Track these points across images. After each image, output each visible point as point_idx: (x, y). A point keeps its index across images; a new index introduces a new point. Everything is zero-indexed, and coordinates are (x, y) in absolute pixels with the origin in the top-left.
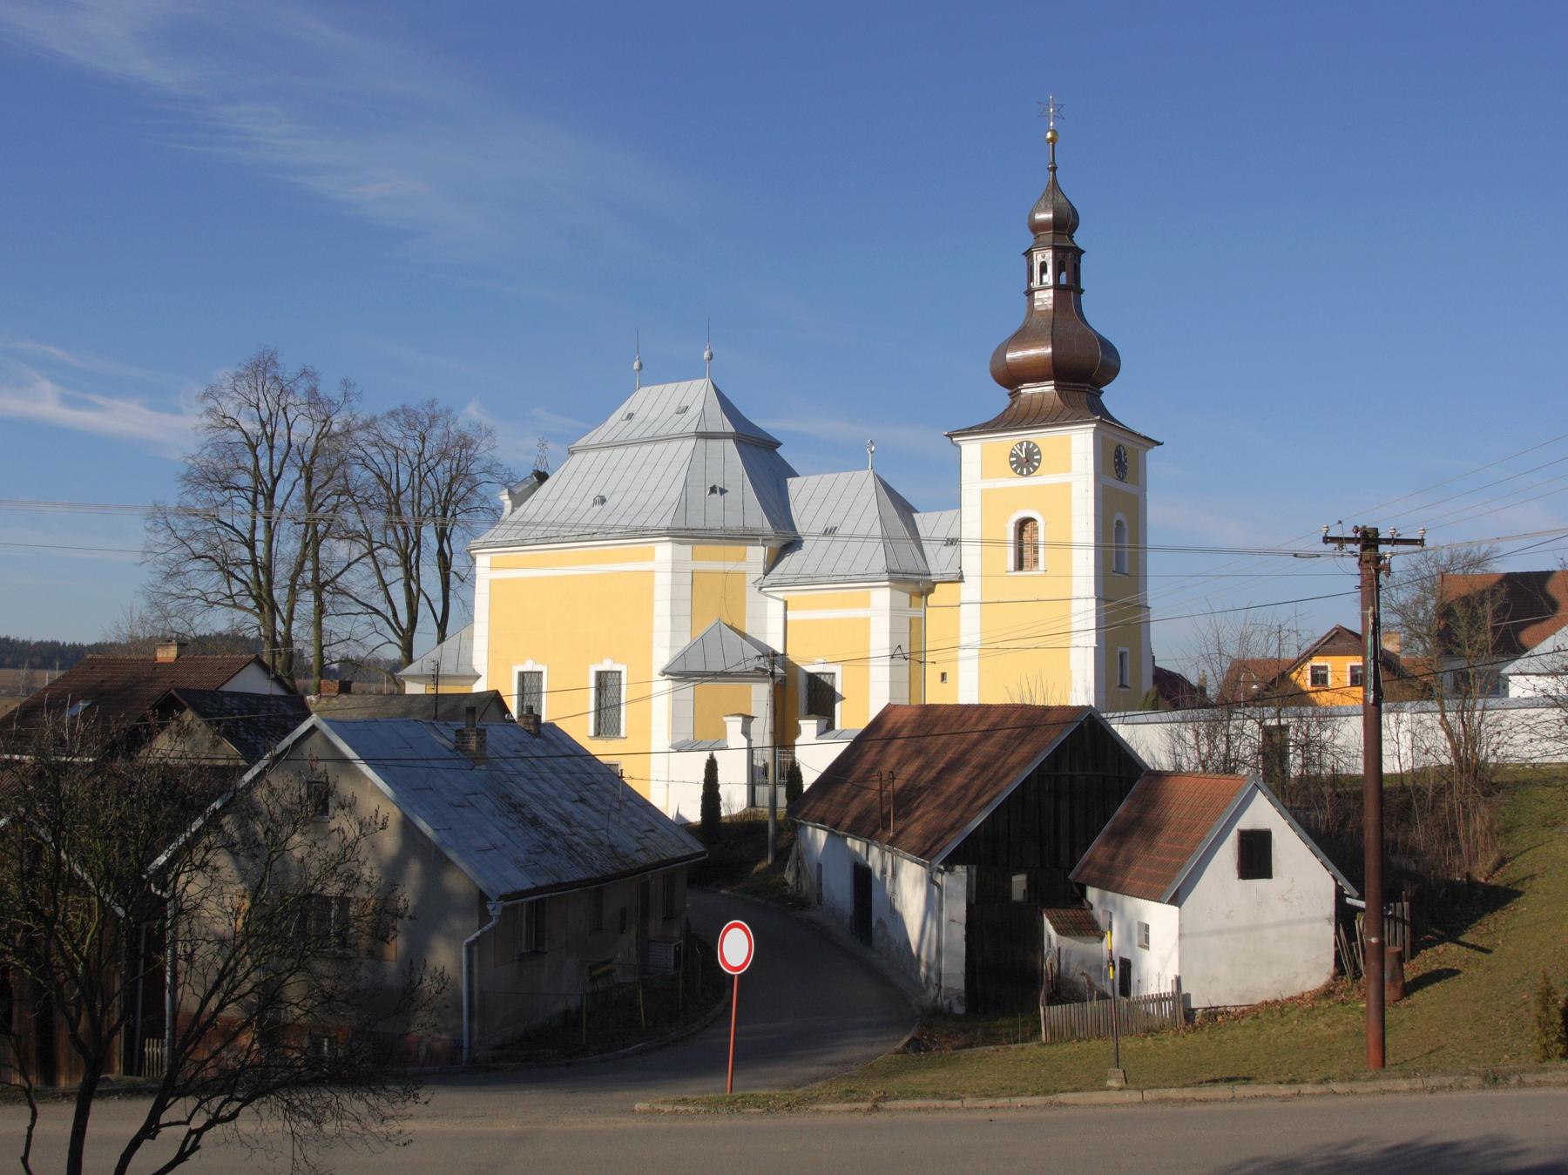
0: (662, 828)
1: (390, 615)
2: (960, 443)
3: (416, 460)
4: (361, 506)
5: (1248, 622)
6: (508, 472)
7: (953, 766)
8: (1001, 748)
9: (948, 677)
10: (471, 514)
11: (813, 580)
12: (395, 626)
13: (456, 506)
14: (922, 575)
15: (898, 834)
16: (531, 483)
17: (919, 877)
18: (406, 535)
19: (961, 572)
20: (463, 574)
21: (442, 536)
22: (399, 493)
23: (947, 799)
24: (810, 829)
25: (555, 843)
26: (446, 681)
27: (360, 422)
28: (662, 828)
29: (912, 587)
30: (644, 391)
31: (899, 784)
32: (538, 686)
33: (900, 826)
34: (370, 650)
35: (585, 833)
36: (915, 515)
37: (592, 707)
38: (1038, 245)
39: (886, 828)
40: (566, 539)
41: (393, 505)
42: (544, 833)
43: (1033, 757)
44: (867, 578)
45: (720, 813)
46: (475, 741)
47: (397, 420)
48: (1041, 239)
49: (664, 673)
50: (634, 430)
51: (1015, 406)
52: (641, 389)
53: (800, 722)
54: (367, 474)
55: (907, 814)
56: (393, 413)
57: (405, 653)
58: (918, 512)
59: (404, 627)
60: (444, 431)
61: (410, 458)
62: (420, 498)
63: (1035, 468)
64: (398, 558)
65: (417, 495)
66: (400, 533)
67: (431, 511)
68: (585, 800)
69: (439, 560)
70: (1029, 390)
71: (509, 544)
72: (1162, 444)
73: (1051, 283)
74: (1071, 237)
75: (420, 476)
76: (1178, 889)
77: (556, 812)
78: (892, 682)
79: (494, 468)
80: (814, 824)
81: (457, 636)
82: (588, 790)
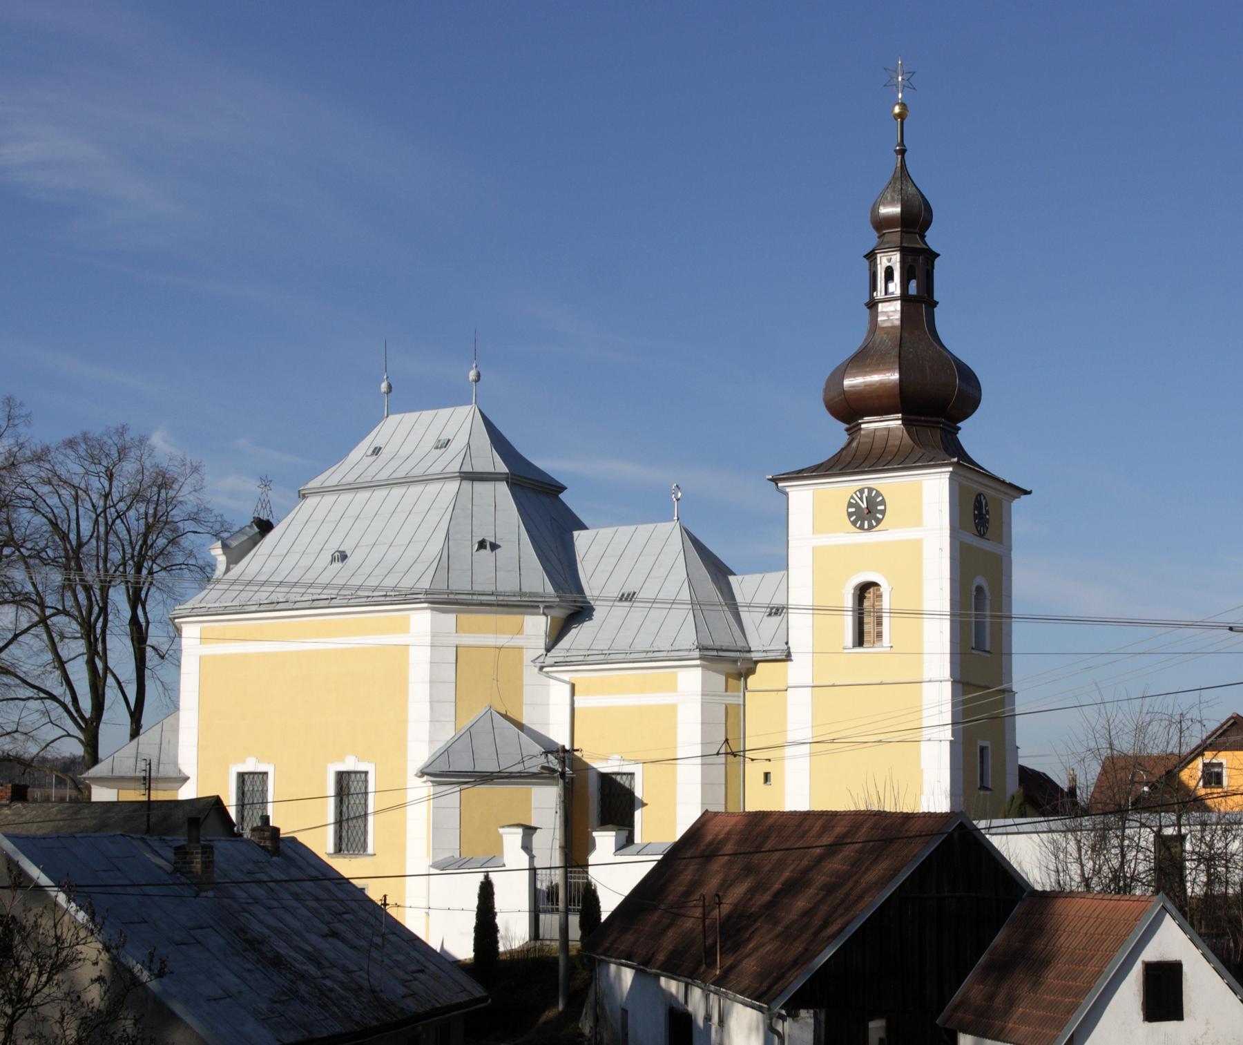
0: (432, 967)
1: (68, 700)
2: (788, 490)
3: (101, 503)
4: (31, 561)
5: (1145, 711)
6: (219, 519)
7: (793, 887)
8: (852, 865)
9: (772, 777)
10: (173, 572)
11: (606, 658)
12: (75, 715)
13: (154, 562)
14: (740, 651)
15: (727, 972)
16: (251, 534)
17: (754, 1024)
18: (89, 599)
19: (789, 648)
20: (163, 648)
21: (136, 600)
22: (80, 545)
23: (786, 928)
24: (613, 967)
25: (303, 989)
26: (160, 785)
27: (28, 453)
28: (432, 967)
29: (729, 667)
30: (394, 419)
31: (726, 908)
32: (262, 791)
33: (729, 961)
34: (44, 745)
35: (341, 976)
36: (732, 579)
37: (331, 817)
38: (883, 246)
39: (712, 964)
40: (297, 606)
41: (72, 559)
42: (289, 976)
43: (893, 876)
44: (676, 657)
45: (498, 948)
46: (199, 860)
47: (76, 451)
48: (887, 238)
49: (422, 774)
50: (381, 469)
51: (854, 444)
52: (390, 416)
53: (594, 834)
54: (38, 520)
55: (735, 948)
56: (71, 441)
57: (89, 749)
58: (735, 574)
59: (88, 715)
60: (137, 466)
61: (94, 501)
62: (106, 553)
63: (879, 521)
64: (78, 628)
65: (102, 548)
66: (82, 596)
67: (121, 569)
68: (337, 934)
69: (132, 630)
70: (871, 425)
71: (225, 611)
72: (1030, 493)
73: (898, 292)
74: (923, 237)
75: (107, 524)
76: (1072, 1035)
77: (302, 950)
78: (703, 784)
79: (202, 515)
80: (618, 961)
81: (158, 727)
82: (340, 921)
